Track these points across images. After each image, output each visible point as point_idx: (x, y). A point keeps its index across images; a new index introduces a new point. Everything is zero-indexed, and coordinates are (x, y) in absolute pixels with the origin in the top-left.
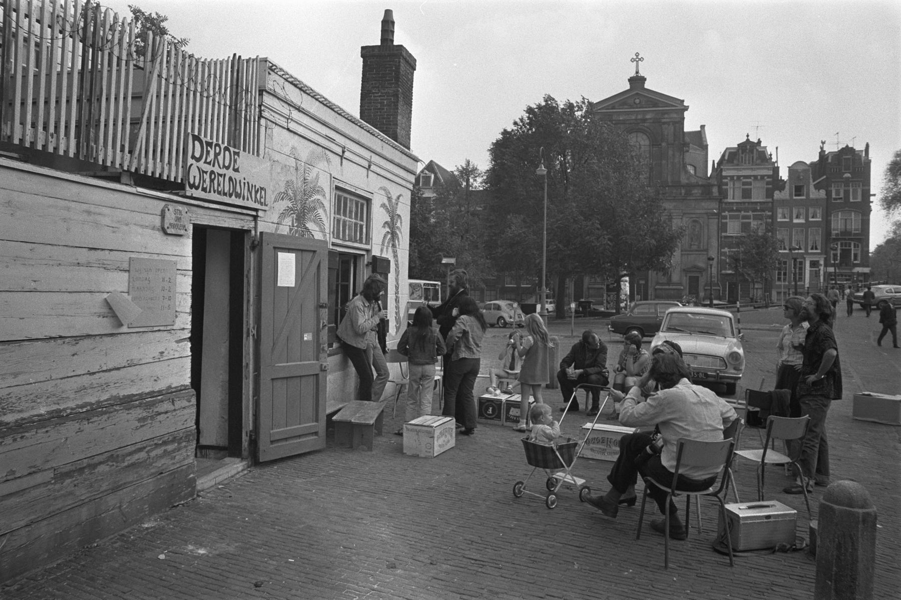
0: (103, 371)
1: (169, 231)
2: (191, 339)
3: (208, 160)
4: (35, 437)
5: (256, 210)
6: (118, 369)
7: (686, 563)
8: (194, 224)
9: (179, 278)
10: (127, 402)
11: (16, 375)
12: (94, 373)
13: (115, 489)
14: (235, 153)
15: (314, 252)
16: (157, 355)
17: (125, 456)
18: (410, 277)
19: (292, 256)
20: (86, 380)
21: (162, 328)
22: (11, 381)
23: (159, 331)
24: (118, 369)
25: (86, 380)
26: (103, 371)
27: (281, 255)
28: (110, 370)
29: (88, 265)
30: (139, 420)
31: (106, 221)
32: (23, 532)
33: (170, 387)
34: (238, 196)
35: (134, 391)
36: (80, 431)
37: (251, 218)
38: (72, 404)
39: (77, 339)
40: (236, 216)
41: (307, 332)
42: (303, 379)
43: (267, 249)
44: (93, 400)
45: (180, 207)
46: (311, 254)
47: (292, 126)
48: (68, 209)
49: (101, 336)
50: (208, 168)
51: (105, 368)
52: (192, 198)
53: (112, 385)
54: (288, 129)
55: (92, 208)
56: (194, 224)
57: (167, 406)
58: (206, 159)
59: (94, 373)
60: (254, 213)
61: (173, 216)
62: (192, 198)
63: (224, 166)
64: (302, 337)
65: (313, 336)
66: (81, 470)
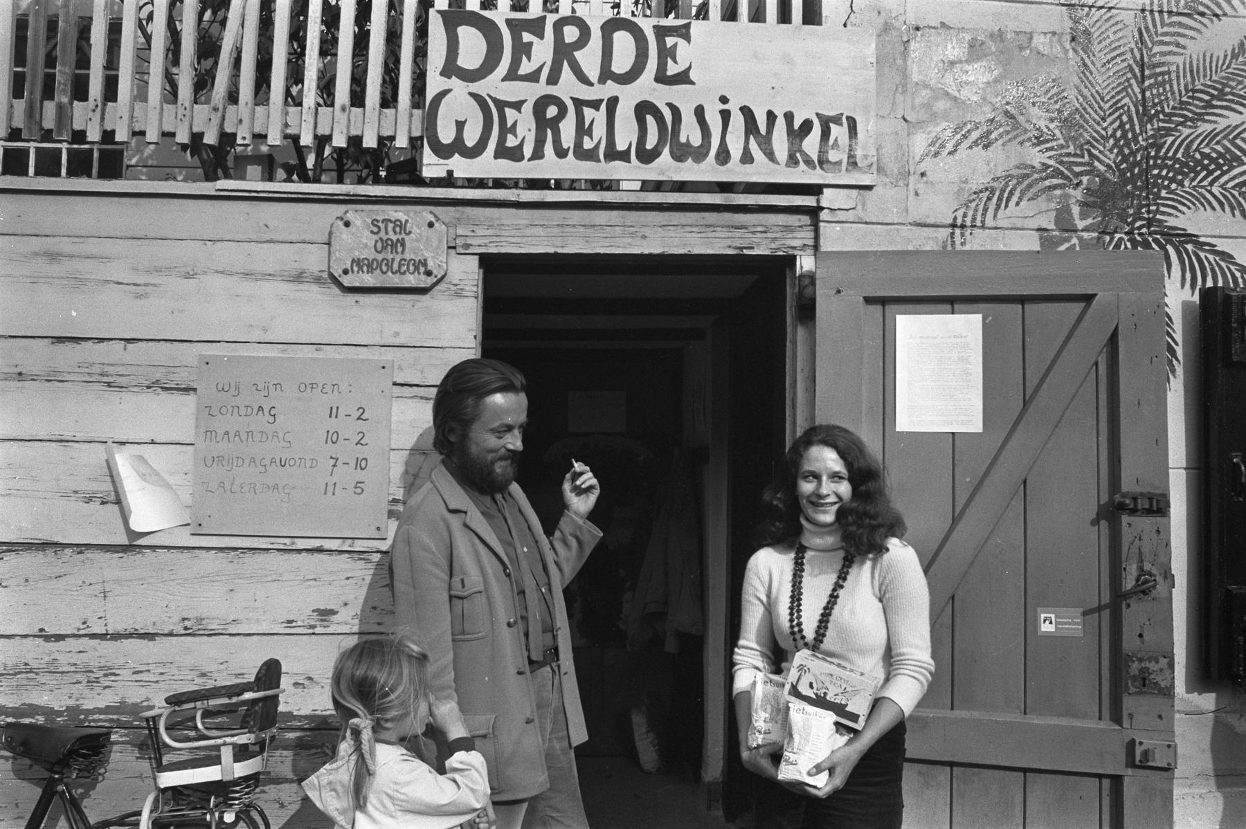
0: (93, 636)
1: (347, 281)
3: (526, 68)
4: (1019, 799)
5: (815, 190)
6: (150, 636)
8: (486, 261)
12: (60, 638)
15: (1088, 299)
18: (58, 175)
19: (968, 327)
21: (328, 544)
23: (320, 550)
24: (150, 636)
26: (93, 636)
28: (117, 637)
34: (682, 153)
37: (806, 219)
40: (711, 217)
41: (1049, 604)
42: (1036, 782)
46: (1077, 307)
49: (81, 548)
51: (99, 630)
52: (449, 181)
53: (126, 674)
55: (66, 246)
56: (486, 261)
58: (515, 63)
59: (60, 638)
60: (809, 201)
61: (369, 240)
63: (607, 74)
64: (1029, 623)
65: (1036, 626)
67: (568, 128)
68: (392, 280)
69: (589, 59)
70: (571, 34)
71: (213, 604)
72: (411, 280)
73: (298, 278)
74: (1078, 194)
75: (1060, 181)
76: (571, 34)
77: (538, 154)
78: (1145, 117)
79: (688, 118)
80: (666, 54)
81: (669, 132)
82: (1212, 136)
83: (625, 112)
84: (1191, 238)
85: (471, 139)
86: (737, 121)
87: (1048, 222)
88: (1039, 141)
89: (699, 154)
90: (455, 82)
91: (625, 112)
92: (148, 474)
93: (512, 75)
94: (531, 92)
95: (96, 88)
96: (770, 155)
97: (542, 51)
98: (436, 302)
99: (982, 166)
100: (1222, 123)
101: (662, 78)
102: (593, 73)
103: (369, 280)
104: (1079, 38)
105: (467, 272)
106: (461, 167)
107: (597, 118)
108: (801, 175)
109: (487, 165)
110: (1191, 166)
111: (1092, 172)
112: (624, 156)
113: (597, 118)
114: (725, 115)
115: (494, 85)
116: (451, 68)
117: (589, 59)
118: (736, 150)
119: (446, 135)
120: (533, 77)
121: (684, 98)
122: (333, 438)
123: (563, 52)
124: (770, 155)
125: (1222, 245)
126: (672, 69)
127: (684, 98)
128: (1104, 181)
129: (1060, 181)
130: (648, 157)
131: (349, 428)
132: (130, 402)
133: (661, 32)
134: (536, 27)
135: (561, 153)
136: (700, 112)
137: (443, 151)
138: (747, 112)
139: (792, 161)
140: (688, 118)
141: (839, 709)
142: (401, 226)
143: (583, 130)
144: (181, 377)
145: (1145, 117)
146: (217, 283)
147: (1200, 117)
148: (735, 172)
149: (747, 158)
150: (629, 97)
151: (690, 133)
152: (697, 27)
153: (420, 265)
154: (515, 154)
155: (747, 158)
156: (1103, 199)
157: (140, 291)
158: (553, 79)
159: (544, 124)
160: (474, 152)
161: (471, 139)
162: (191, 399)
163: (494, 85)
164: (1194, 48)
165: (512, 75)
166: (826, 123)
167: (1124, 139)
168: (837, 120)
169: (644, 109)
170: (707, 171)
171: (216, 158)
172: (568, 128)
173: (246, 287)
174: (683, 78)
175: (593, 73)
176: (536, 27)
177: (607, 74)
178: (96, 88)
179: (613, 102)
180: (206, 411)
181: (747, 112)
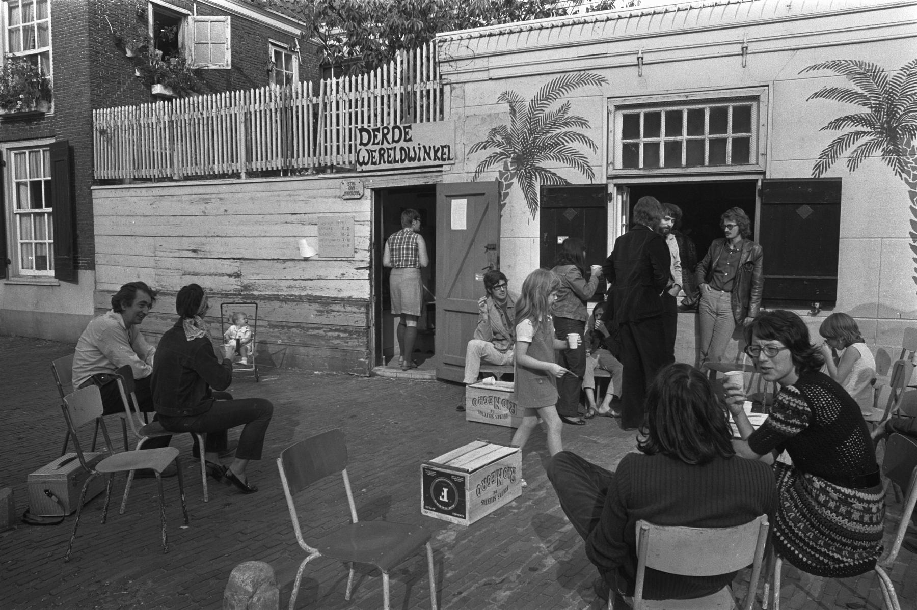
2: (370, 268)
5: (441, 166)
7: (20, 439)
8: (372, 189)
9: (357, 227)
10: (312, 299)
11: (258, 274)
13: (305, 345)
14: (405, 128)
16: (339, 275)
17: (308, 329)
19: (464, 202)
20: (292, 283)
22: (255, 277)
25: (292, 283)
27: (454, 202)
29: (292, 223)
30: (318, 311)
31: (301, 198)
32: (30, 292)
33: (350, 297)
34: (411, 159)
35: (318, 294)
36: (281, 307)
38: (285, 293)
39: (285, 261)
43: (440, 197)
44: (297, 294)
45: (353, 180)
47: (495, 74)
48: (279, 195)
50: (377, 147)
52: (362, 171)
54: (491, 79)
55: (292, 193)
57: (336, 307)
62: (362, 171)
63: (394, 141)
66: (283, 327)
67: (386, 156)
68: (353, 196)
69: (389, 137)
70: (386, 131)
71: (322, 273)
72: (356, 196)
73: (335, 197)
74: (510, 160)
75: (869, 129)
76: (386, 131)
77: (380, 163)
78: (531, 134)
79: (411, 150)
80: (406, 133)
81: (407, 155)
82: (551, 138)
83: (398, 150)
84: (543, 169)
85: (366, 160)
86: (422, 150)
87: (502, 169)
88: (499, 145)
89: (414, 159)
90: (362, 147)
91: (398, 150)
92: (309, 245)
93: (374, 144)
94: (377, 147)
95: (295, 156)
96: (430, 158)
97: (380, 136)
98: (363, 201)
99: (484, 154)
100: (555, 133)
101: (405, 140)
102: (390, 141)
103: (348, 197)
104: (513, 111)
105: (368, 193)
106: (364, 168)
107: (392, 152)
108: (437, 162)
109: (370, 167)
110: (544, 148)
111: (515, 152)
112: (398, 162)
113: (392, 152)
114: (420, 148)
115: (370, 147)
116: (361, 143)
117: (389, 137)
118: (422, 158)
119: (361, 160)
120: (378, 144)
121: (410, 145)
122: (343, 234)
123: (384, 136)
124: (430, 158)
125: (553, 171)
126: (408, 138)
127: (410, 145)
128: (518, 155)
129: (869, 129)
130: (403, 161)
131: (346, 232)
132: (306, 227)
133: (405, 128)
134: (378, 130)
135: (384, 162)
136: (414, 148)
137: (361, 164)
138: (424, 147)
139: (435, 160)
140: (411, 150)
141: (470, 473)
142: (353, 183)
143: (389, 156)
144: (314, 222)
145: (531, 134)
146: (320, 199)
147: (548, 132)
148: (422, 163)
149: (425, 159)
150: (398, 146)
151: (412, 154)
152: (413, 125)
153: (358, 193)
154: (374, 164)
155: (425, 159)
156: (519, 161)
157: (306, 202)
158: (382, 144)
159: (381, 155)
160: (366, 164)
161: (366, 160)
162: (316, 227)
163: (370, 147)
164: (547, 111)
165: (374, 144)
166: (443, 147)
167: (525, 141)
168: (445, 146)
169: (402, 149)
170: (416, 164)
171: (320, 169)
172: (386, 156)
173: (325, 200)
174: (410, 140)
175: (390, 141)
176: (378, 130)
177: (394, 141)
178: (295, 156)
179: (395, 148)
180: (319, 229)
181: (424, 147)
